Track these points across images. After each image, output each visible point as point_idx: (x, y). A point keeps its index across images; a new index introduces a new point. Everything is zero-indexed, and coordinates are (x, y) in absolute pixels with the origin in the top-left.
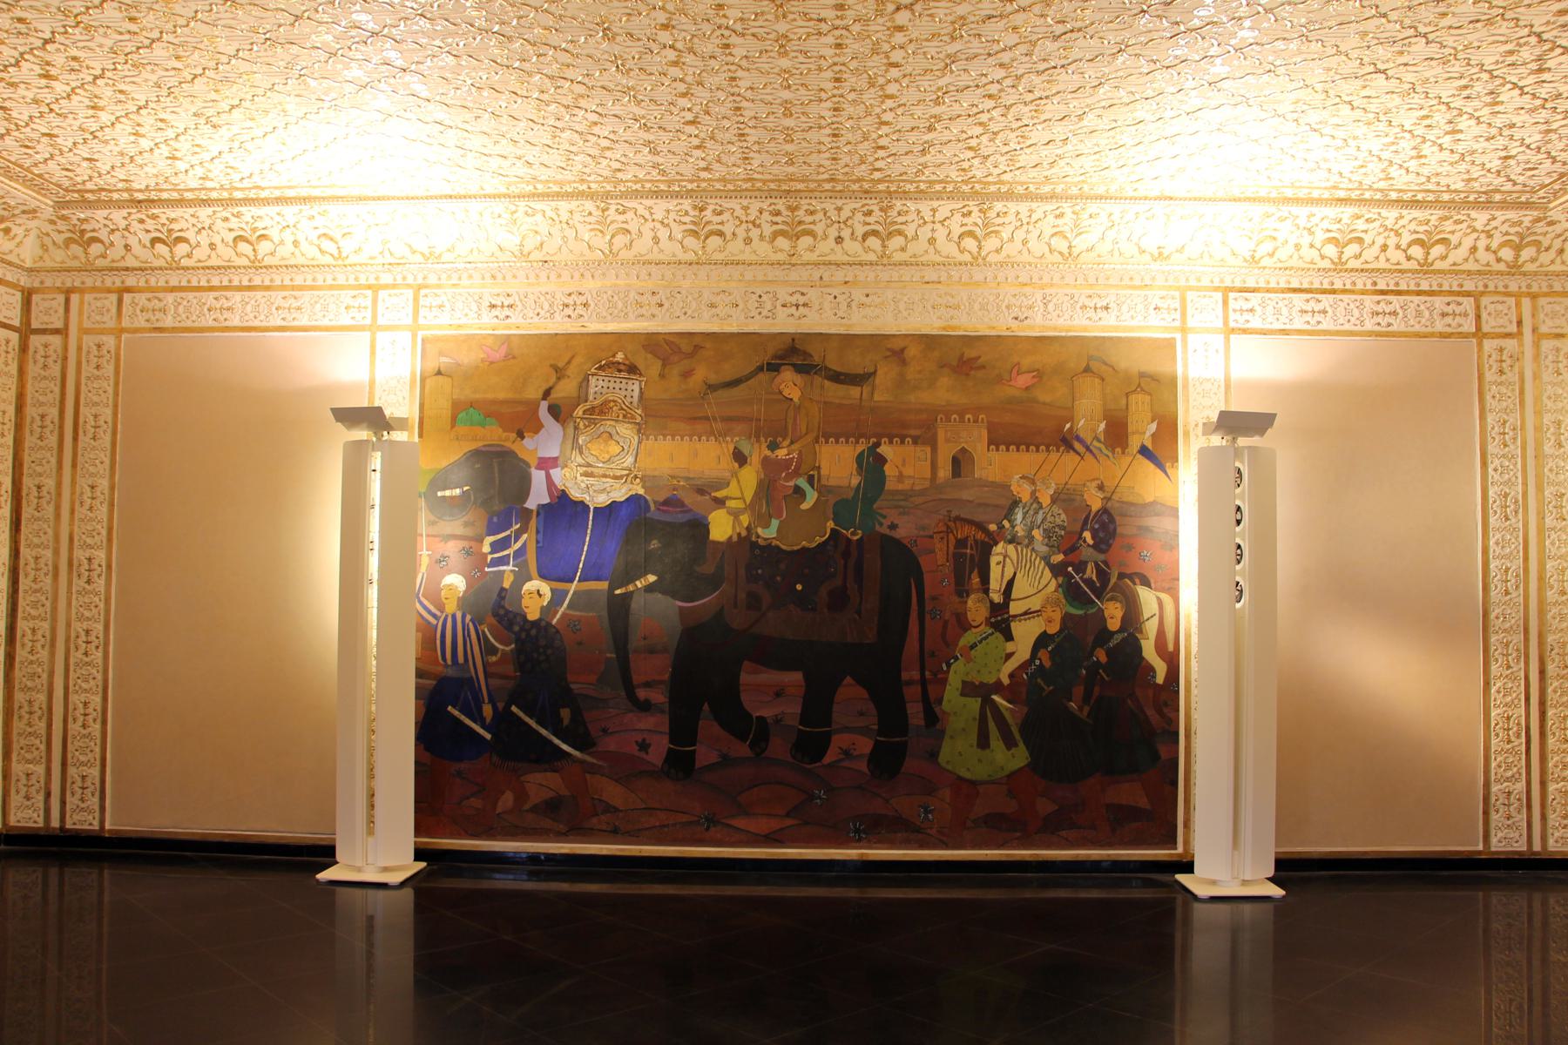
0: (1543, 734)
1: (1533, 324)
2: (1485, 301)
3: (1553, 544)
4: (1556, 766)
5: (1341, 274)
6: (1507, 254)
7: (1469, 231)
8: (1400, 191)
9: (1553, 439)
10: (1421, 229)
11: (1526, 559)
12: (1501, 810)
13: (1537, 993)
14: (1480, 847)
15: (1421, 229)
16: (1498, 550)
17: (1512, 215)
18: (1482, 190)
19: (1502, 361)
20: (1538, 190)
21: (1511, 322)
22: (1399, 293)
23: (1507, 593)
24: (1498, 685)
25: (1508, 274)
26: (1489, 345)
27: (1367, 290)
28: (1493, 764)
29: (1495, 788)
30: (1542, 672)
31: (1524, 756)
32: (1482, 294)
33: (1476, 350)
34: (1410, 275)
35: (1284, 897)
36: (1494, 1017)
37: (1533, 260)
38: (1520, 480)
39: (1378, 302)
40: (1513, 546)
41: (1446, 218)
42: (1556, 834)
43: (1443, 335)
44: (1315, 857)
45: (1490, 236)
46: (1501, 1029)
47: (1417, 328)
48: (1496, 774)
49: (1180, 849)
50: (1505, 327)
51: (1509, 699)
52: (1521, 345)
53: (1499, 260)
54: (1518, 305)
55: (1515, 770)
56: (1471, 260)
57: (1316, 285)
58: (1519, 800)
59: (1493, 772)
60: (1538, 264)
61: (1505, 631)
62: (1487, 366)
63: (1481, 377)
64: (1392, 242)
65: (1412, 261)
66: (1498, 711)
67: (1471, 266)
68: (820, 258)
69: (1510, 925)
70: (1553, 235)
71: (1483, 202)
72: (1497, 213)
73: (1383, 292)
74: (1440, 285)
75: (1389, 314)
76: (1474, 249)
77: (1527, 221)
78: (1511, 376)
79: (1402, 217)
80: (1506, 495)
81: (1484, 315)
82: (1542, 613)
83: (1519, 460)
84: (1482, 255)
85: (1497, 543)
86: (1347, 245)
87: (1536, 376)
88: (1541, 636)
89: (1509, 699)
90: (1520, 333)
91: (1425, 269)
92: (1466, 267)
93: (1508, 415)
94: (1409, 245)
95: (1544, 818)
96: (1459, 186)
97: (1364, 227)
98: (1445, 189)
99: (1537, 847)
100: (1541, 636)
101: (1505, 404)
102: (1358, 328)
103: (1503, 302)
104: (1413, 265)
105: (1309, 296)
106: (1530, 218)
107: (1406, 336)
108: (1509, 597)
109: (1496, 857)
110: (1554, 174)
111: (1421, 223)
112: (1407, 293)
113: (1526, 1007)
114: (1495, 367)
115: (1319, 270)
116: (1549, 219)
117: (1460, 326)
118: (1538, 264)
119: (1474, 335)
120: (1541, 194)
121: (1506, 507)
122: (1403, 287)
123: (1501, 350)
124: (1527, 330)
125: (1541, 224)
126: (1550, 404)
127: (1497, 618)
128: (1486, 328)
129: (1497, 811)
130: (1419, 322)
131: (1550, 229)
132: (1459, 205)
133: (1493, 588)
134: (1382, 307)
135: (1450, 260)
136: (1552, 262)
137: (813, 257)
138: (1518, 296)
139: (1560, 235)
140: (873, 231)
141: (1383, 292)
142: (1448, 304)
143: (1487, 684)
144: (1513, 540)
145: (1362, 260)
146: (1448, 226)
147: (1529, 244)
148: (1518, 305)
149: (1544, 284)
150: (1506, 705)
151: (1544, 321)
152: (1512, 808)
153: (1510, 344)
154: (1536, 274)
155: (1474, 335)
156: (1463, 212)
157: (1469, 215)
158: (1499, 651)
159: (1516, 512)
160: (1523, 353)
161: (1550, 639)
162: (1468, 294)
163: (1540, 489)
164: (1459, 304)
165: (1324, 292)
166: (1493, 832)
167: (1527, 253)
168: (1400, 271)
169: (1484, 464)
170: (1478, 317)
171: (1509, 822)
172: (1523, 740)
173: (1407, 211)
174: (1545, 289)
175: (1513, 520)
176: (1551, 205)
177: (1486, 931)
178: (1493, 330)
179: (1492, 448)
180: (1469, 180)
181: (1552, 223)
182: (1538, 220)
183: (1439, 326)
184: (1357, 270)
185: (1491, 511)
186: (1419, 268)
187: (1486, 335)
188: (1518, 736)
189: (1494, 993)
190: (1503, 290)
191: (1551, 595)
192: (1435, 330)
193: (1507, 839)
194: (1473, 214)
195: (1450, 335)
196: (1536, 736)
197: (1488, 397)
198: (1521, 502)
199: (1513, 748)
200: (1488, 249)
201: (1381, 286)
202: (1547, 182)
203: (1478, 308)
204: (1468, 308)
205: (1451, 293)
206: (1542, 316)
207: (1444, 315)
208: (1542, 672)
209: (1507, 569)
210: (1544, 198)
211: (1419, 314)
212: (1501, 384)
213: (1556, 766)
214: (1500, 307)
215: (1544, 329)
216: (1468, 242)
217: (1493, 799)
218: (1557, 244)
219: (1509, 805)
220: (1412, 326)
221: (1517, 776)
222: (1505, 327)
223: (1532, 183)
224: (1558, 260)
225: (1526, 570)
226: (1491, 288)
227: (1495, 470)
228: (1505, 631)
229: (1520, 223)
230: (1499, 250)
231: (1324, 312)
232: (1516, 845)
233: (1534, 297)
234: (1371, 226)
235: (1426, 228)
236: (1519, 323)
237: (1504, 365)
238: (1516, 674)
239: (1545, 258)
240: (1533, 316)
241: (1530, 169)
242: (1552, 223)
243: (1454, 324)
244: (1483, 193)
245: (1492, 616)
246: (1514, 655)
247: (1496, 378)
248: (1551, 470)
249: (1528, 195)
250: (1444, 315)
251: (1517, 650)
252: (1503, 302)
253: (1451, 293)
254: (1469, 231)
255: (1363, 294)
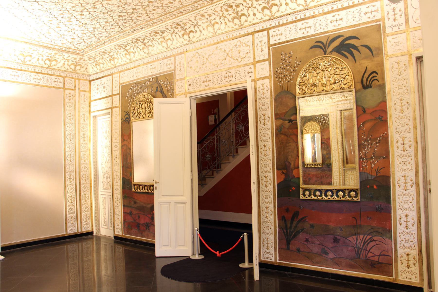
0: (80, 200)
1: (79, 87)
2: (66, 79)
3: (82, 148)
4: (84, 208)
5: (24, 65)
6: (73, 67)
7: (63, 59)
8: (43, 43)
9: (83, 119)
10: (74, 61)
11: (75, 152)
12: (70, 222)
13: (81, 270)
14: (65, 233)
15: (74, 61)
16: (68, 149)
17: (74, 56)
18: (67, 47)
19: (70, 96)
20: (81, 50)
21: (73, 86)
22: (42, 73)
23: (70, 161)
24: (68, 187)
25: (73, 73)
26: (67, 91)
27: (32, 71)
28: (68, 209)
29: (68, 216)
30: (80, 183)
31: (75, 206)
32: (66, 77)
33: (63, 93)
34: (45, 69)
35: (4, 259)
36: (70, 279)
37: (79, 70)
38: (74, 130)
39: (36, 75)
40: (72, 148)
41: (57, 54)
42: (84, 226)
43: (54, 87)
44: (16, 244)
45: (68, 61)
46: (72, 282)
47: (47, 84)
48: (68, 212)
49: (394, 277)
50: (71, 87)
51: (71, 191)
52: (75, 92)
53: (70, 68)
54: (75, 81)
55: (73, 210)
56: (63, 67)
57: (16, 67)
58: (75, 218)
59: (68, 211)
60: (80, 71)
61: (70, 172)
62: (66, 97)
63: (64, 100)
64: (41, 58)
65: (46, 65)
66: (69, 194)
67: (63, 69)
68: (81, 72)
69: (73, 253)
70: (84, 64)
71: (67, 51)
72: (71, 55)
73: (37, 73)
74: (54, 73)
75: (39, 79)
76: (64, 64)
77: (78, 58)
78: (72, 101)
79: (70, 56)
80: (70, 134)
81: (66, 83)
82: (79, 166)
83: (74, 124)
84: (66, 66)
85: (68, 147)
86: (27, 56)
87: (79, 102)
88: (79, 173)
89: (71, 191)
90: (75, 89)
91: (50, 68)
92: (61, 69)
93: (71, 111)
94: (46, 60)
95: (81, 222)
96: (60, 45)
97: (83, 62)
98: (56, 45)
99: (80, 231)
100: (79, 173)
101: (70, 108)
102: (29, 82)
103: (71, 80)
104: (46, 66)
105: (14, 70)
106: (79, 58)
107: (43, 86)
108: (71, 162)
109: (69, 235)
110: (85, 46)
111: (49, 54)
112: (44, 74)
113: (78, 275)
114: (68, 98)
115: (17, 63)
116: (84, 59)
117: (59, 85)
118: (80, 71)
119: (63, 88)
120: (82, 51)
121: (70, 137)
122: (43, 72)
123: (85, 95)
124: (77, 88)
125: (82, 60)
126: (82, 110)
127: (68, 168)
128: (66, 87)
129: (69, 222)
130: (48, 83)
131: (84, 62)
132: (60, 50)
133: (67, 159)
134: (14, 74)
135: (57, 66)
136: (84, 71)
137: (30, 63)
138: (75, 79)
139: (86, 64)
140: (56, 60)
141: (37, 73)
142: (56, 79)
143: (65, 187)
144: (72, 146)
145: (31, 62)
146: (57, 56)
147: (78, 65)
148: (75, 81)
149: (82, 77)
150: (70, 193)
151: (81, 87)
152: (73, 221)
153: (72, 92)
154: (80, 73)
155: (63, 88)
156: (61, 53)
157: (63, 54)
158: (69, 177)
159: (73, 139)
160: (76, 95)
161: (82, 173)
162: (62, 77)
163: (79, 132)
164: (59, 79)
165: (19, 70)
166: (68, 228)
167: (78, 68)
168: (43, 67)
169: (65, 125)
170: (64, 83)
171: (72, 225)
172: (75, 202)
173: (71, 55)
174: (82, 78)
175: (72, 141)
176: (84, 55)
177: (67, 256)
178: (68, 88)
179: (67, 121)
180: (63, 43)
181: (84, 60)
182: (81, 59)
183: (53, 85)
184: (29, 65)
185: (66, 138)
186: (48, 67)
187: (66, 89)
188: (88, 199)
189: (70, 273)
190: (59, 75)
191: (82, 162)
192: (52, 86)
193: (72, 230)
194: (64, 54)
195: (56, 88)
196: (78, 200)
197: (66, 106)
198: (74, 136)
199: (73, 204)
200: (68, 65)
201: (37, 71)
202: (83, 48)
203: (64, 81)
204: (62, 80)
205: (57, 76)
206: (81, 85)
207: (55, 82)
208: (80, 183)
209: (70, 155)
210: (82, 53)
211: (48, 80)
212: (70, 103)
213: (84, 208)
214: (70, 81)
215: (81, 89)
216: (62, 62)
217: (68, 219)
218: (86, 66)
219: (72, 220)
220: (45, 84)
221: (74, 212)
222: (71, 87)
223: (79, 48)
224: (86, 71)
225: (75, 155)
226: (68, 76)
227: (68, 127)
228: (70, 172)
229: (76, 59)
230: (71, 65)
231: (18, 76)
232: (88, 229)
233: (79, 80)
234: (60, 57)
235: (76, 60)
236: (75, 86)
237: (71, 98)
238: (73, 184)
239: (83, 70)
240: (79, 85)
241: (79, 44)
242: (84, 60)
243: (57, 85)
244: (67, 48)
245: (67, 168)
246: (72, 178)
247: (69, 101)
248: (82, 127)
249: (78, 51)
250: (55, 82)
251: (73, 177)
252: (71, 80)
253: (57, 76)
254: (63, 59)
255: (31, 72)
